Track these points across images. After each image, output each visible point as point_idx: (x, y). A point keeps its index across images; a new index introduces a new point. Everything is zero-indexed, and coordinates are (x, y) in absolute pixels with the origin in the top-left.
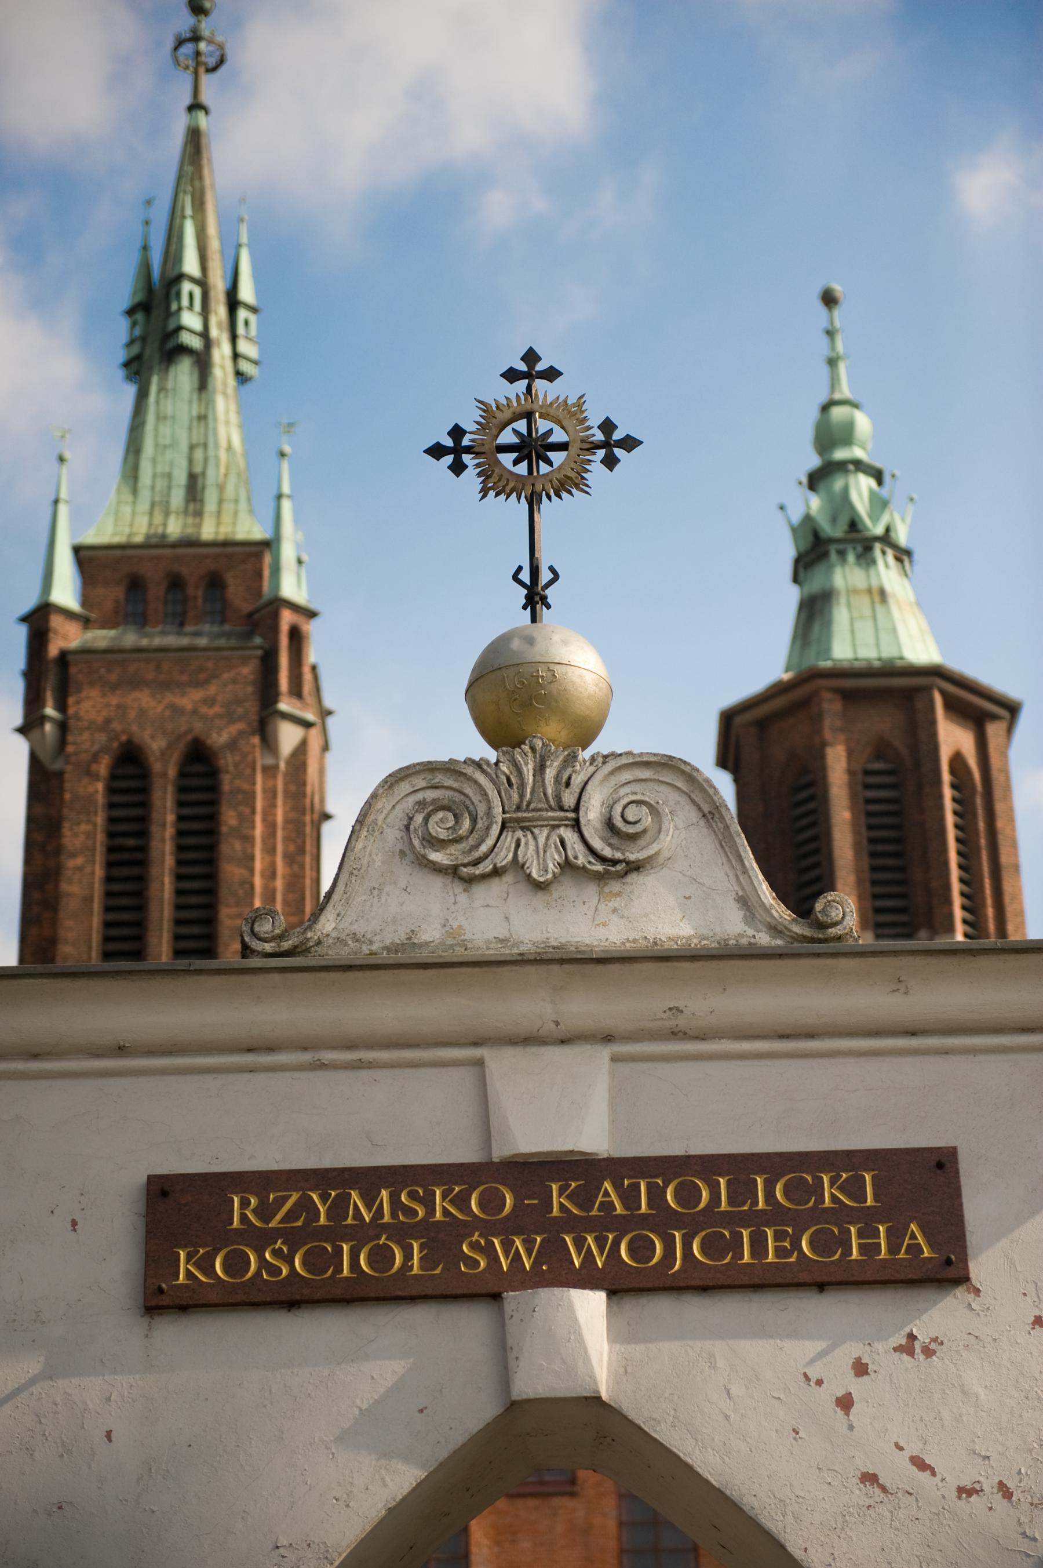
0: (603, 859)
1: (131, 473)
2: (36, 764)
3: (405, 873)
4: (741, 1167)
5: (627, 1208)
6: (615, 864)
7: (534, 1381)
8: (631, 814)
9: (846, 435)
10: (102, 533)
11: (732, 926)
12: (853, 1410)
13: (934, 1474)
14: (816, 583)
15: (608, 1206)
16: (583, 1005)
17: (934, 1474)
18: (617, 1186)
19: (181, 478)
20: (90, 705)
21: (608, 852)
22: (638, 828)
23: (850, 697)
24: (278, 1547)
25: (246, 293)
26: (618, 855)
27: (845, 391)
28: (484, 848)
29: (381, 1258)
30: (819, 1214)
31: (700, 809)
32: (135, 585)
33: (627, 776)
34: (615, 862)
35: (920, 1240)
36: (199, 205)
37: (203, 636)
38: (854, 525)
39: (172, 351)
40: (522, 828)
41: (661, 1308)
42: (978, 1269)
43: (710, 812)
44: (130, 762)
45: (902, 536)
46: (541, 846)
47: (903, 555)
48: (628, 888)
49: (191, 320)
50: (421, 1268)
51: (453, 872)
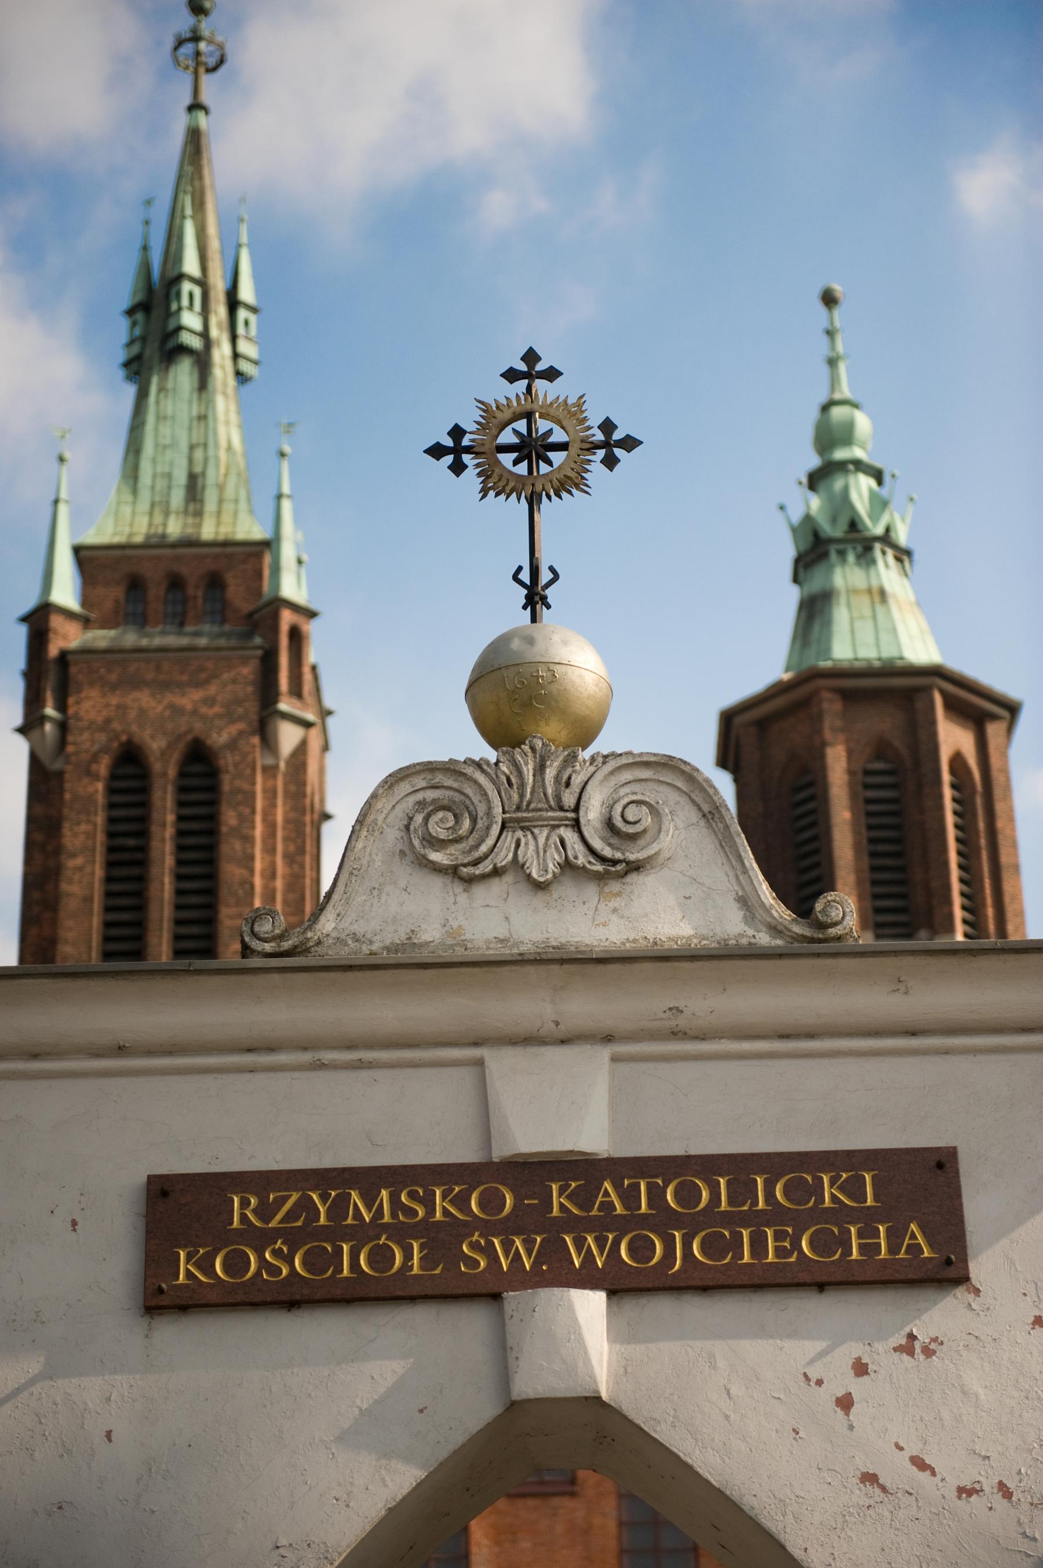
0: (603, 859)
1: (131, 473)
2: (36, 764)
3: (405, 873)
4: (741, 1167)
5: (627, 1208)
6: (615, 864)
7: (534, 1381)
8: (631, 814)
9: (846, 435)
10: (102, 533)
11: (732, 926)
12: (853, 1410)
13: (934, 1474)
14: (816, 583)
15: (608, 1206)
16: (583, 1005)
17: (934, 1474)
18: (617, 1186)
19: (181, 478)
20: (90, 705)
21: (608, 852)
22: (638, 828)
23: (850, 697)
24: (278, 1547)
25: (246, 293)
26: (618, 855)
27: (845, 391)
28: (484, 848)
29: (381, 1258)
30: (819, 1214)
31: (700, 809)
32: (135, 585)
33: (627, 776)
34: (615, 862)
35: (920, 1240)
36: (199, 205)
37: (203, 636)
38: (854, 525)
39: (172, 351)
40: (522, 828)
41: (661, 1308)
42: (978, 1269)
43: (710, 812)
44: (130, 762)
45: (902, 536)
46: (541, 846)
47: (903, 555)
48: (628, 888)
49: (191, 320)
50: (421, 1268)
51: (453, 872)
